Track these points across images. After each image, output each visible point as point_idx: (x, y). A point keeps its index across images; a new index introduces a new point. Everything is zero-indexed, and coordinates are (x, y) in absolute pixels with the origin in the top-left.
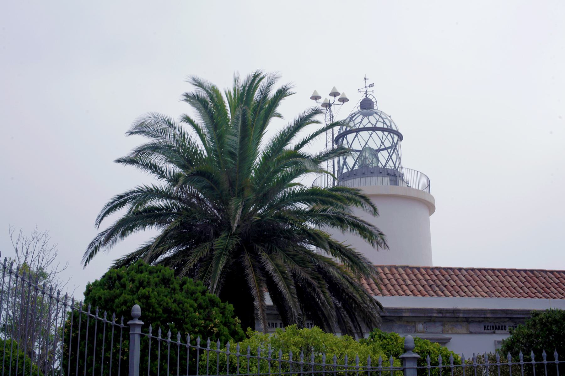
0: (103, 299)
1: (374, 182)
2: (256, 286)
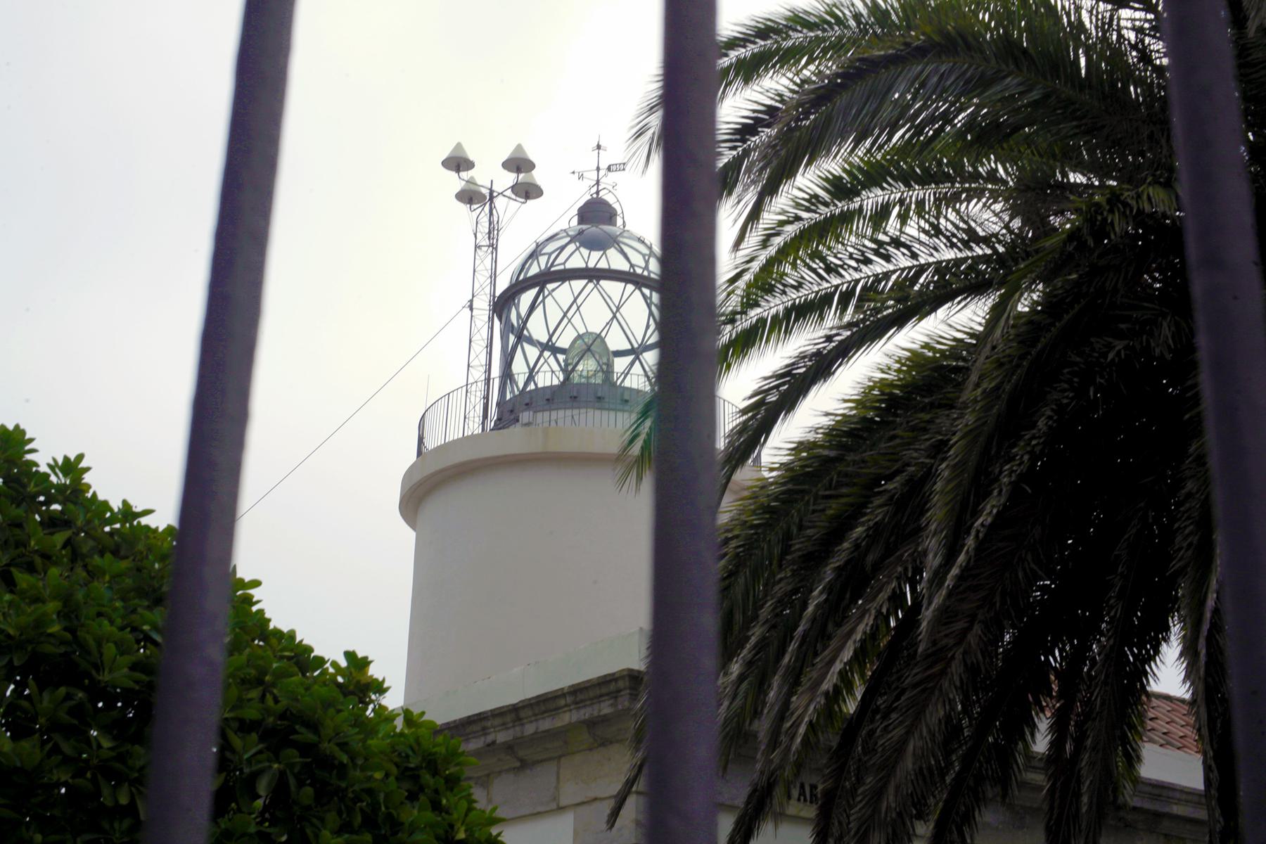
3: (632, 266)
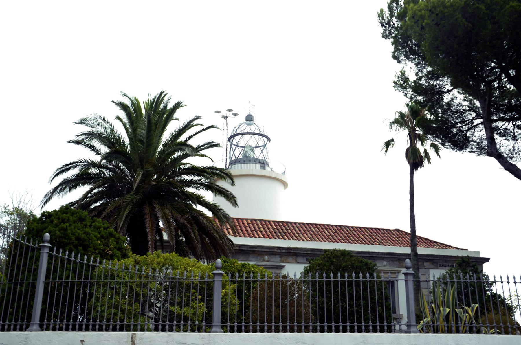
0: (35, 230)
1: (252, 167)
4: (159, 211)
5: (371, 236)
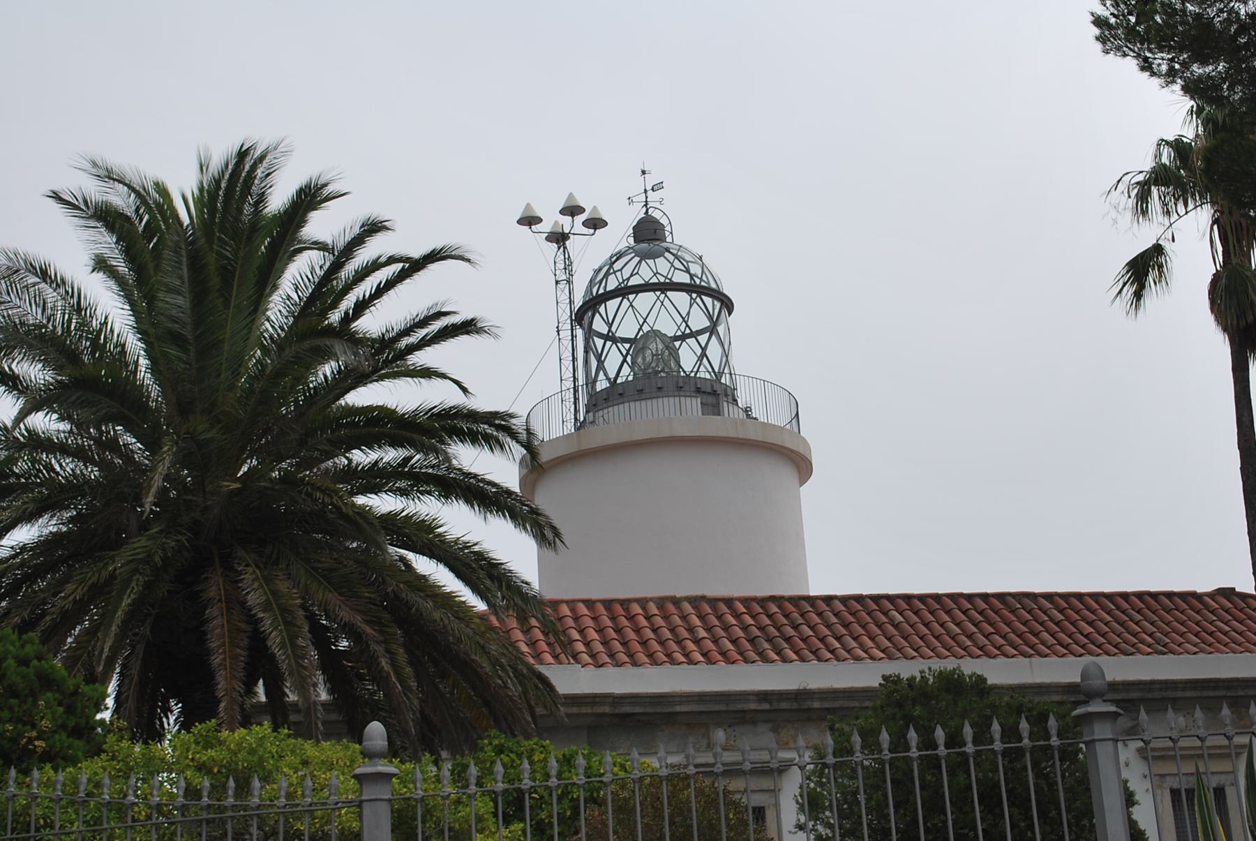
2: (224, 645)
3: (692, 276)
4: (256, 585)
5: (1122, 624)
